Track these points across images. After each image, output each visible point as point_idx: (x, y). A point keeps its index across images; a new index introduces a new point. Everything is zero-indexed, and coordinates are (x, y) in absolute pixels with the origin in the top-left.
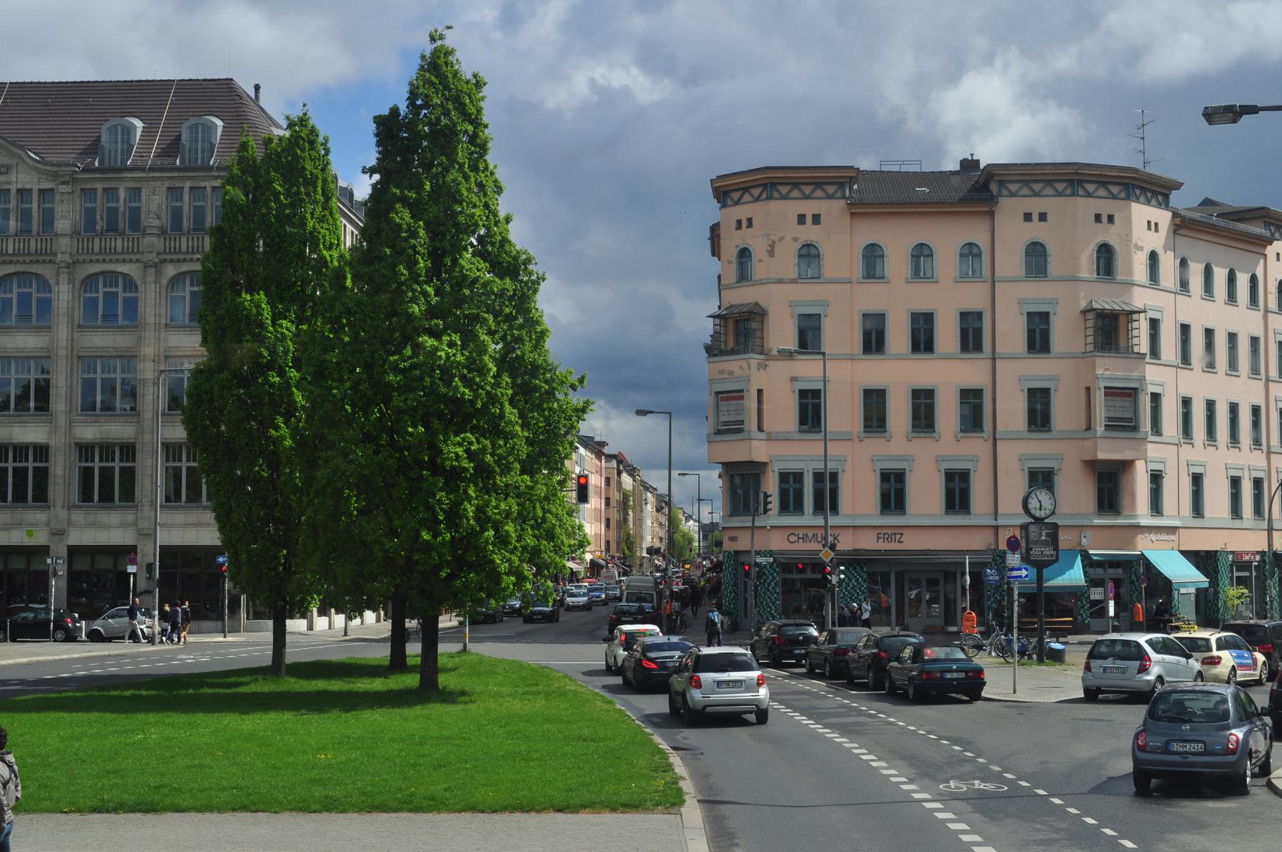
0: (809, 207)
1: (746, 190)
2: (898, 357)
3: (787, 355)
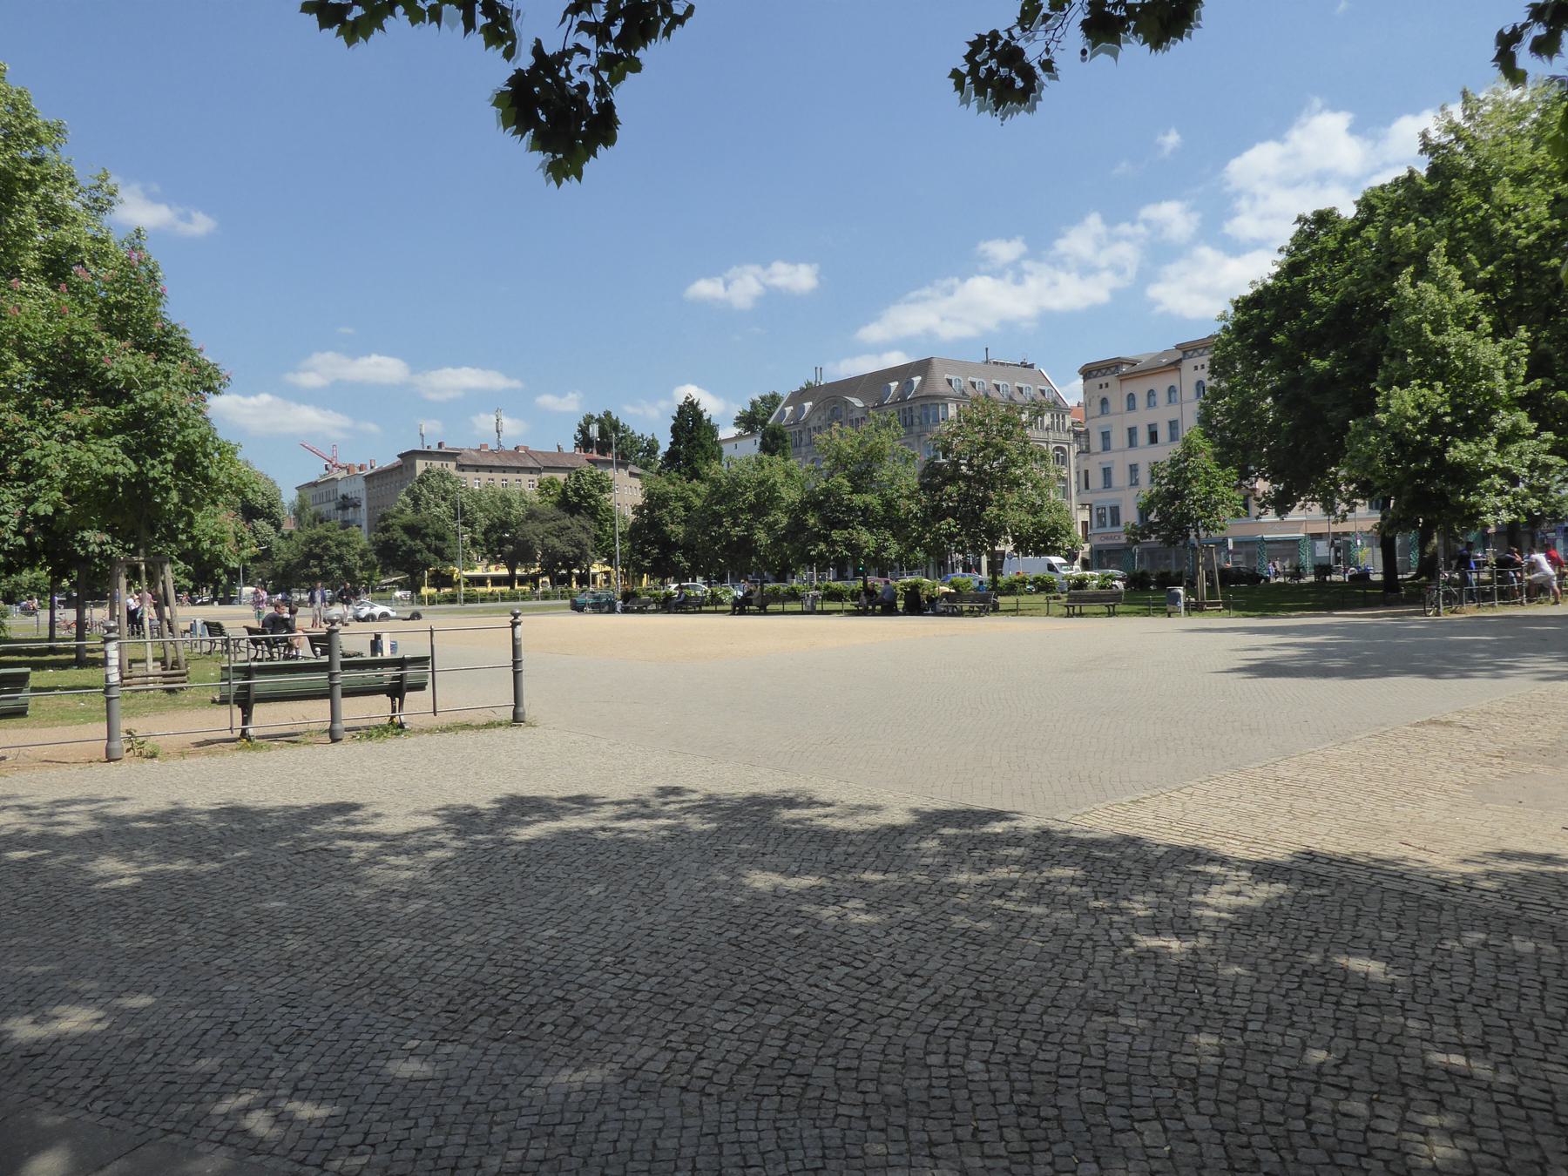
0: (1103, 380)
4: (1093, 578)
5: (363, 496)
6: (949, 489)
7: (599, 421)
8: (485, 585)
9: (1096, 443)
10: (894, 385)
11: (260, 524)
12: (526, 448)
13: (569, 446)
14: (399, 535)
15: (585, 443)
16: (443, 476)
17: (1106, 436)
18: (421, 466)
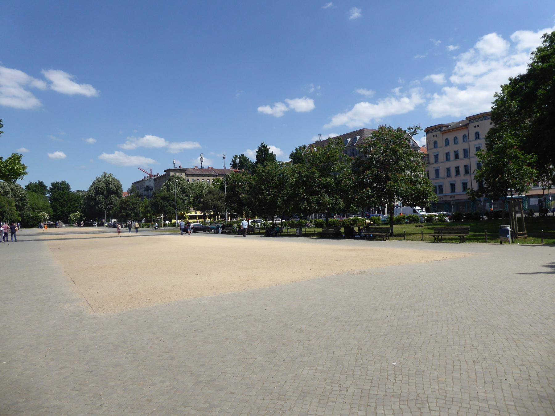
0: (435, 134)
1: (479, 118)
2: (452, 161)
3: (433, 164)
4: (436, 216)
5: (153, 186)
6: (367, 172)
7: (240, 158)
8: (196, 219)
9: (432, 159)
10: (349, 140)
11: (113, 196)
12: (212, 168)
13: (228, 167)
14: (159, 200)
15: (234, 165)
16: (178, 178)
17: (436, 157)
18: (172, 174)
